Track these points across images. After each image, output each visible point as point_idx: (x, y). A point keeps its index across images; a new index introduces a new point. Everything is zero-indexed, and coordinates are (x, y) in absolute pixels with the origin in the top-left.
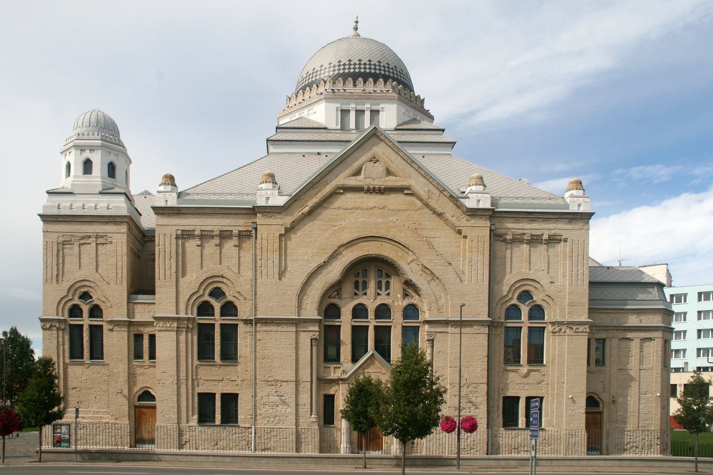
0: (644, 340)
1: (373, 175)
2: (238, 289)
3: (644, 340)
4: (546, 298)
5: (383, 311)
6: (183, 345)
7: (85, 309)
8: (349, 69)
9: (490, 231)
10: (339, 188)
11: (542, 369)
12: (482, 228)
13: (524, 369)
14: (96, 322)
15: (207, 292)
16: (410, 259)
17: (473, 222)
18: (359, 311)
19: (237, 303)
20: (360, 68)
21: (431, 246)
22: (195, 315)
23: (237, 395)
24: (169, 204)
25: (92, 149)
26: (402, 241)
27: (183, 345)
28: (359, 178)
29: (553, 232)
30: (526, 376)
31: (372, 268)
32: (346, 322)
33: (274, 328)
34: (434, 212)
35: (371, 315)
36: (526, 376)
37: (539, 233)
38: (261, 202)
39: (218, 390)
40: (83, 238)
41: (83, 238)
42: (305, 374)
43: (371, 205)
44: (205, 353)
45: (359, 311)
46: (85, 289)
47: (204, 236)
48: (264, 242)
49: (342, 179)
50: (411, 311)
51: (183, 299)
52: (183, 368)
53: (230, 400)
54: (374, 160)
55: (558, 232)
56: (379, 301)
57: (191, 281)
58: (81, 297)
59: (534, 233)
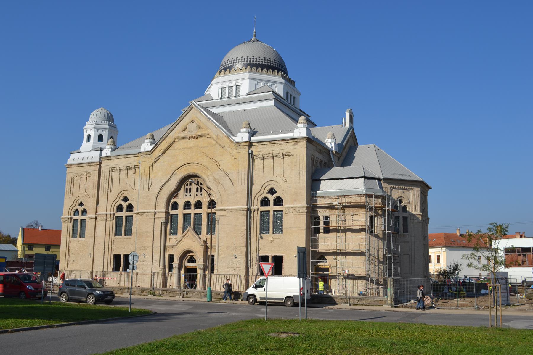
5: (199, 205)
8: (247, 61)
15: (121, 199)
16: (209, 174)
18: (187, 205)
20: (253, 61)
21: (218, 165)
22: (72, 216)
25: (103, 129)
28: (185, 132)
44: (118, 233)
48: (143, 171)
50: (212, 204)
54: (193, 121)
58: (269, 192)
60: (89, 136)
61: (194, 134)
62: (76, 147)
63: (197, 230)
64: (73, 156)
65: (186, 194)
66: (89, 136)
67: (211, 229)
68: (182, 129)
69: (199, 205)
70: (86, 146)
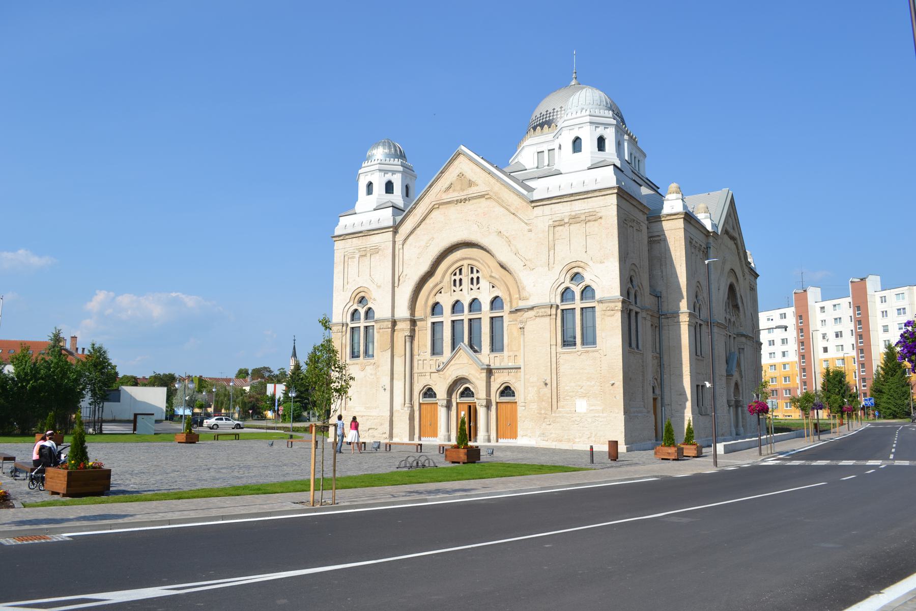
5: (474, 304)
18: (456, 306)
19: (594, 286)
25: (394, 172)
44: (568, 342)
60: (370, 185)
62: (348, 207)
63: (474, 346)
64: (343, 221)
65: (472, 286)
66: (370, 185)
67: (496, 345)
68: (443, 189)
69: (474, 304)
70: (364, 202)
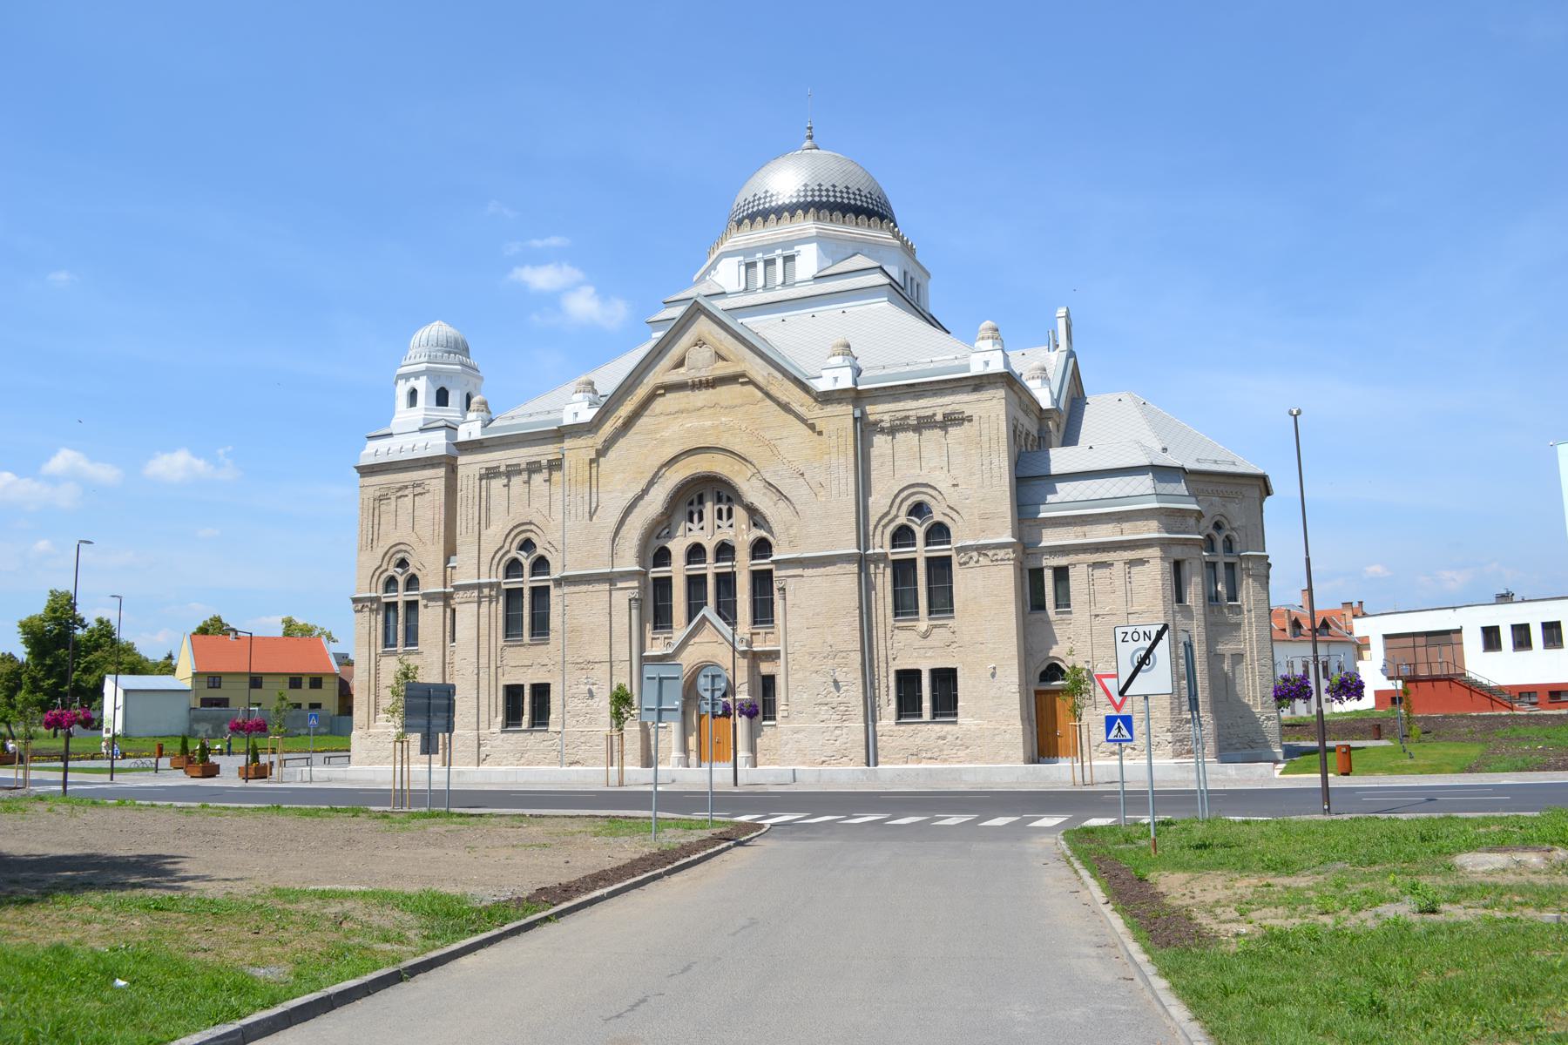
0: (1132, 563)
1: (701, 365)
2: (549, 538)
3: (1132, 563)
4: (948, 511)
6: (484, 621)
7: (401, 580)
9: (855, 419)
10: (658, 388)
11: (950, 622)
12: (843, 416)
13: (923, 624)
14: (938, 550)
17: (831, 409)
18: (696, 552)
19: (548, 556)
23: (548, 685)
24: (473, 437)
25: (417, 375)
26: (736, 449)
27: (484, 621)
28: (682, 370)
29: (948, 410)
30: (925, 636)
31: (703, 492)
32: (678, 571)
33: (583, 588)
34: (779, 403)
35: (710, 556)
36: (925, 636)
37: (929, 412)
38: (568, 420)
39: (527, 679)
40: (400, 489)
41: (400, 489)
42: (622, 651)
43: (700, 404)
44: (512, 626)
45: (696, 552)
46: (400, 555)
47: (512, 471)
49: (661, 374)
50: (761, 548)
51: (485, 559)
52: (484, 652)
53: (945, 679)
54: (700, 343)
55: (957, 408)
56: (718, 538)
57: (495, 533)
59: (922, 413)
61: (706, 373)
63: (727, 611)
67: (763, 612)
